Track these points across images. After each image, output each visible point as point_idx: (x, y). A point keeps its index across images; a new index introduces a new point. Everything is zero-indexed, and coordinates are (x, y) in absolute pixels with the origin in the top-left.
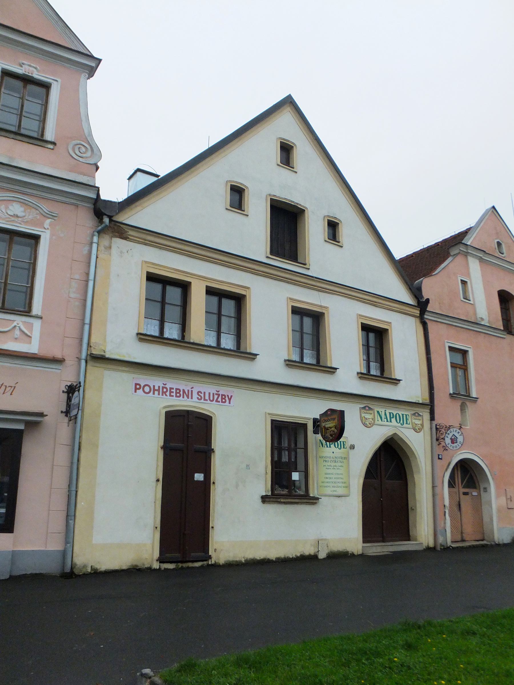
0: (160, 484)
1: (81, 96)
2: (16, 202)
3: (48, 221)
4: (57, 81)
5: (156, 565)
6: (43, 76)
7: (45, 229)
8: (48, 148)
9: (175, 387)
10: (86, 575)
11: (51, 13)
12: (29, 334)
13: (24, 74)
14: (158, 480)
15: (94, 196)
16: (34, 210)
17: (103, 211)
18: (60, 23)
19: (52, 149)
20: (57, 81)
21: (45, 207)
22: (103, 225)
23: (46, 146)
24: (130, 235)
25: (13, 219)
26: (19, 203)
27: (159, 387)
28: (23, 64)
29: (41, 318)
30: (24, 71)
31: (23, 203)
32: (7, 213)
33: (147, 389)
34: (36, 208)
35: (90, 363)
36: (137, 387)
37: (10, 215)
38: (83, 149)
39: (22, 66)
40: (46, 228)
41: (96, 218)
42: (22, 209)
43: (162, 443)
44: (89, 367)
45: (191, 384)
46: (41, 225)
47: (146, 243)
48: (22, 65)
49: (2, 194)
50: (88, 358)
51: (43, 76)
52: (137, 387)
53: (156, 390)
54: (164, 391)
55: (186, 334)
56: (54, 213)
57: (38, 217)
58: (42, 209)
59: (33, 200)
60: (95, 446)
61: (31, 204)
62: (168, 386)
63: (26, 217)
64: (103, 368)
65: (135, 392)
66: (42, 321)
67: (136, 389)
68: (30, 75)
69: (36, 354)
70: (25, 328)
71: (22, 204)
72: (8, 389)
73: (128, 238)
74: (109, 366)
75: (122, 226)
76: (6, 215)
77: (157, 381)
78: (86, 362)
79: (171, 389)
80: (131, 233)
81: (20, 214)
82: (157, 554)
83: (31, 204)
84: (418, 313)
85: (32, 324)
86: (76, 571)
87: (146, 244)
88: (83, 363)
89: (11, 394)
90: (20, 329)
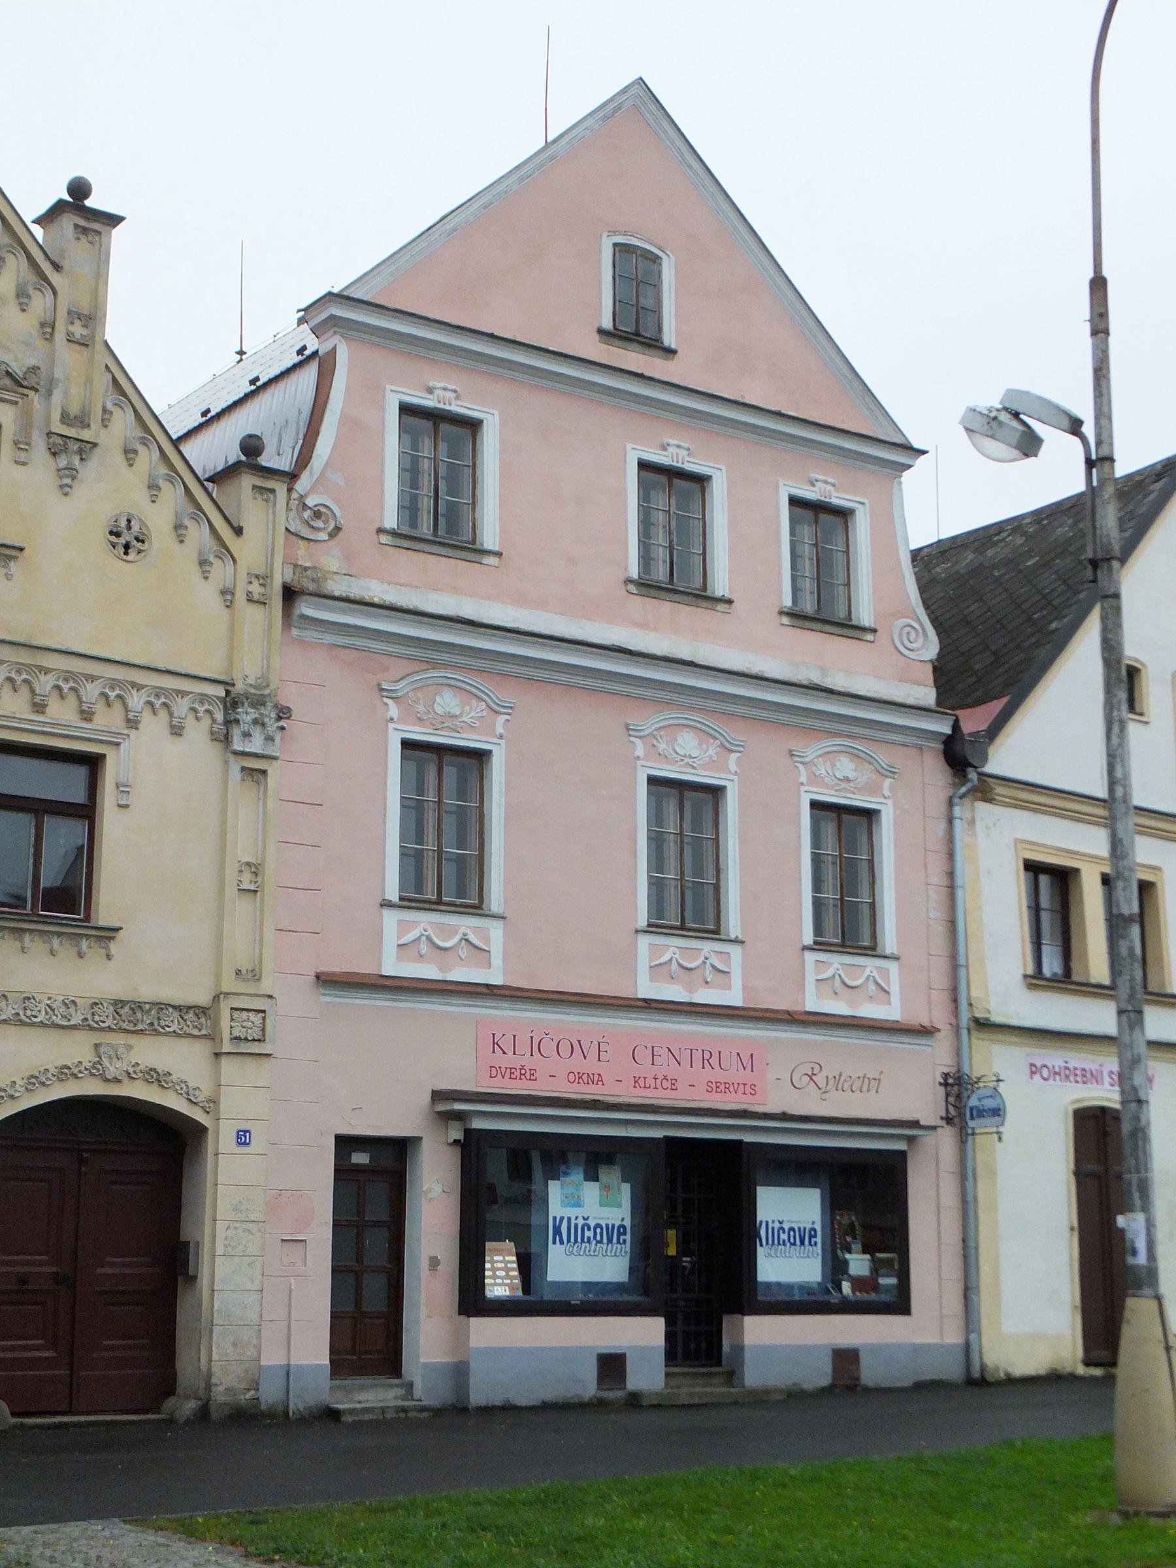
0: (1076, 1235)
1: (898, 526)
2: (844, 754)
3: (888, 782)
4: (863, 504)
5: (1081, 1370)
6: (844, 499)
7: (885, 798)
8: (866, 641)
9: (1079, 1065)
10: (999, 1383)
11: (811, 323)
12: (887, 988)
13: (819, 500)
14: (1072, 1229)
15: (948, 730)
16: (867, 765)
17: (971, 761)
18: (856, 383)
19: (873, 642)
20: (863, 504)
21: (884, 757)
22: (969, 785)
23: (864, 638)
24: (999, 795)
25: (843, 785)
26: (847, 755)
27: (1060, 1067)
28: (816, 481)
29: (503, 918)
30: (819, 495)
31: (854, 755)
32: (835, 776)
33: (1045, 1073)
34: (871, 760)
35: (975, 1034)
36: (1034, 1070)
37: (839, 779)
38: (913, 635)
39: (813, 485)
40: (886, 795)
41: (948, 768)
42: (852, 766)
43: (1072, 1166)
44: (974, 1040)
45: (1100, 1059)
46: (875, 790)
47: (1019, 804)
48: (815, 482)
49: (826, 742)
50: (972, 1024)
51: (844, 499)
52: (1034, 1070)
53: (506, 1265)
54: (1065, 1074)
55: (1074, 965)
56: (894, 768)
57: (874, 778)
58: (877, 761)
59: (864, 747)
60: (993, 1173)
61: (863, 755)
62: (1071, 1066)
63: (859, 780)
64: (990, 1040)
65: (1032, 1078)
66: (743, 951)
67: (1033, 1073)
68: (827, 500)
69: (898, 1021)
70: (880, 977)
71: (853, 757)
72: (873, 1082)
73: (995, 800)
74: (1000, 1037)
75: (988, 780)
76: (834, 778)
77: (1055, 1057)
78: (969, 1032)
79: (1076, 1069)
80: (999, 790)
81: (851, 775)
82: (1080, 1353)
83: (863, 755)
84: (1115, 1102)
85: (887, 971)
86: (989, 1377)
87: (1016, 807)
88: (964, 1032)
89: (877, 1092)
90: (877, 983)
